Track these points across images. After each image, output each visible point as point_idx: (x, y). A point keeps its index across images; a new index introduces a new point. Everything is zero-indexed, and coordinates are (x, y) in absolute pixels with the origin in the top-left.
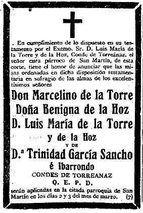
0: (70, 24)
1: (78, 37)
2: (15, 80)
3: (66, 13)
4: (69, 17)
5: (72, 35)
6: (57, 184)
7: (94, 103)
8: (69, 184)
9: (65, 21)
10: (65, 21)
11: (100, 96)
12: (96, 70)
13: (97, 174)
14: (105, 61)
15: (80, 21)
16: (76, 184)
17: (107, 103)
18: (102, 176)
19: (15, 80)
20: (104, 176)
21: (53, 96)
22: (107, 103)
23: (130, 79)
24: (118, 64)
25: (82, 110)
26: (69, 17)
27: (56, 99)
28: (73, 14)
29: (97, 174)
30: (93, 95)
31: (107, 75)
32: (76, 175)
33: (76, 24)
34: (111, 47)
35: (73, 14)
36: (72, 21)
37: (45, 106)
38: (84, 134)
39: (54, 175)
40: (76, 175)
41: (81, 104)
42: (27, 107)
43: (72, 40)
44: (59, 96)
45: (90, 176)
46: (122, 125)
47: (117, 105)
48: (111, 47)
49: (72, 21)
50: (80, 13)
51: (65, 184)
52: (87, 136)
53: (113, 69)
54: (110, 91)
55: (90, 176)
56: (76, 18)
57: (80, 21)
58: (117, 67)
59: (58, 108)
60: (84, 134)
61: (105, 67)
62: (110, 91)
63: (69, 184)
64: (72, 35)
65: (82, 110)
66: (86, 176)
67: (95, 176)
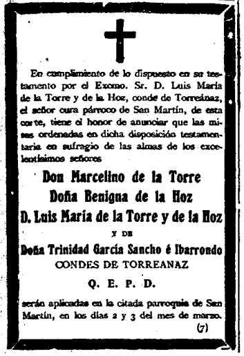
0: (115, 30)
1: (130, 64)
2: (27, 148)
3: (108, 21)
4: (113, 29)
5: (120, 58)
6: (96, 287)
7: (148, 187)
8: (117, 286)
9: (108, 35)
10: (108, 35)
11: (157, 178)
12: (160, 129)
13: (163, 262)
14: (175, 111)
15: (132, 35)
16: (128, 287)
17: (167, 187)
18: (172, 266)
19: (27, 148)
20: (174, 266)
21: (97, 178)
22: (167, 187)
23: (25, 304)
24: (198, 117)
25: (131, 198)
26: (113, 29)
27: (101, 181)
28: (120, 23)
29: (163, 262)
30: (148, 177)
31: (127, 140)
32: (128, 264)
33: (126, 41)
34: (199, 83)
35: (120, 23)
36: (120, 35)
37: (88, 192)
38: (174, 191)
39: (93, 265)
40: (128, 264)
41: (128, 187)
42: (64, 194)
43: (119, 67)
44: (104, 178)
45: (152, 265)
46: (145, 218)
47: (179, 191)
48: (199, 83)
49: (120, 35)
50: (132, 21)
51: (110, 286)
52: (178, 194)
53: (190, 128)
54: (130, 212)
55: (152, 265)
56: (126, 29)
57: (132, 35)
58: (196, 123)
59: (103, 195)
60: (174, 191)
61: (176, 124)
62: (172, 172)
63: (117, 286)
64: (120, 58)
65: (131, 198)
66: (144, 265)
67: (159, 264)
